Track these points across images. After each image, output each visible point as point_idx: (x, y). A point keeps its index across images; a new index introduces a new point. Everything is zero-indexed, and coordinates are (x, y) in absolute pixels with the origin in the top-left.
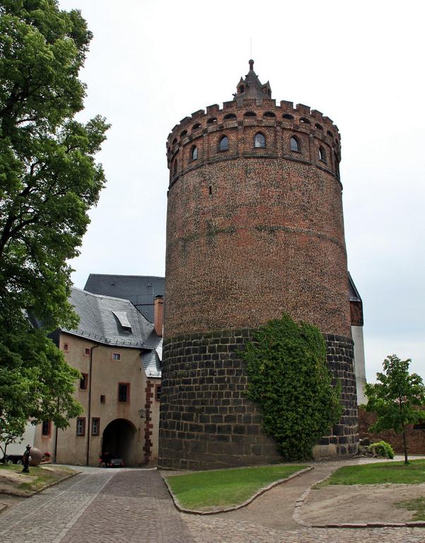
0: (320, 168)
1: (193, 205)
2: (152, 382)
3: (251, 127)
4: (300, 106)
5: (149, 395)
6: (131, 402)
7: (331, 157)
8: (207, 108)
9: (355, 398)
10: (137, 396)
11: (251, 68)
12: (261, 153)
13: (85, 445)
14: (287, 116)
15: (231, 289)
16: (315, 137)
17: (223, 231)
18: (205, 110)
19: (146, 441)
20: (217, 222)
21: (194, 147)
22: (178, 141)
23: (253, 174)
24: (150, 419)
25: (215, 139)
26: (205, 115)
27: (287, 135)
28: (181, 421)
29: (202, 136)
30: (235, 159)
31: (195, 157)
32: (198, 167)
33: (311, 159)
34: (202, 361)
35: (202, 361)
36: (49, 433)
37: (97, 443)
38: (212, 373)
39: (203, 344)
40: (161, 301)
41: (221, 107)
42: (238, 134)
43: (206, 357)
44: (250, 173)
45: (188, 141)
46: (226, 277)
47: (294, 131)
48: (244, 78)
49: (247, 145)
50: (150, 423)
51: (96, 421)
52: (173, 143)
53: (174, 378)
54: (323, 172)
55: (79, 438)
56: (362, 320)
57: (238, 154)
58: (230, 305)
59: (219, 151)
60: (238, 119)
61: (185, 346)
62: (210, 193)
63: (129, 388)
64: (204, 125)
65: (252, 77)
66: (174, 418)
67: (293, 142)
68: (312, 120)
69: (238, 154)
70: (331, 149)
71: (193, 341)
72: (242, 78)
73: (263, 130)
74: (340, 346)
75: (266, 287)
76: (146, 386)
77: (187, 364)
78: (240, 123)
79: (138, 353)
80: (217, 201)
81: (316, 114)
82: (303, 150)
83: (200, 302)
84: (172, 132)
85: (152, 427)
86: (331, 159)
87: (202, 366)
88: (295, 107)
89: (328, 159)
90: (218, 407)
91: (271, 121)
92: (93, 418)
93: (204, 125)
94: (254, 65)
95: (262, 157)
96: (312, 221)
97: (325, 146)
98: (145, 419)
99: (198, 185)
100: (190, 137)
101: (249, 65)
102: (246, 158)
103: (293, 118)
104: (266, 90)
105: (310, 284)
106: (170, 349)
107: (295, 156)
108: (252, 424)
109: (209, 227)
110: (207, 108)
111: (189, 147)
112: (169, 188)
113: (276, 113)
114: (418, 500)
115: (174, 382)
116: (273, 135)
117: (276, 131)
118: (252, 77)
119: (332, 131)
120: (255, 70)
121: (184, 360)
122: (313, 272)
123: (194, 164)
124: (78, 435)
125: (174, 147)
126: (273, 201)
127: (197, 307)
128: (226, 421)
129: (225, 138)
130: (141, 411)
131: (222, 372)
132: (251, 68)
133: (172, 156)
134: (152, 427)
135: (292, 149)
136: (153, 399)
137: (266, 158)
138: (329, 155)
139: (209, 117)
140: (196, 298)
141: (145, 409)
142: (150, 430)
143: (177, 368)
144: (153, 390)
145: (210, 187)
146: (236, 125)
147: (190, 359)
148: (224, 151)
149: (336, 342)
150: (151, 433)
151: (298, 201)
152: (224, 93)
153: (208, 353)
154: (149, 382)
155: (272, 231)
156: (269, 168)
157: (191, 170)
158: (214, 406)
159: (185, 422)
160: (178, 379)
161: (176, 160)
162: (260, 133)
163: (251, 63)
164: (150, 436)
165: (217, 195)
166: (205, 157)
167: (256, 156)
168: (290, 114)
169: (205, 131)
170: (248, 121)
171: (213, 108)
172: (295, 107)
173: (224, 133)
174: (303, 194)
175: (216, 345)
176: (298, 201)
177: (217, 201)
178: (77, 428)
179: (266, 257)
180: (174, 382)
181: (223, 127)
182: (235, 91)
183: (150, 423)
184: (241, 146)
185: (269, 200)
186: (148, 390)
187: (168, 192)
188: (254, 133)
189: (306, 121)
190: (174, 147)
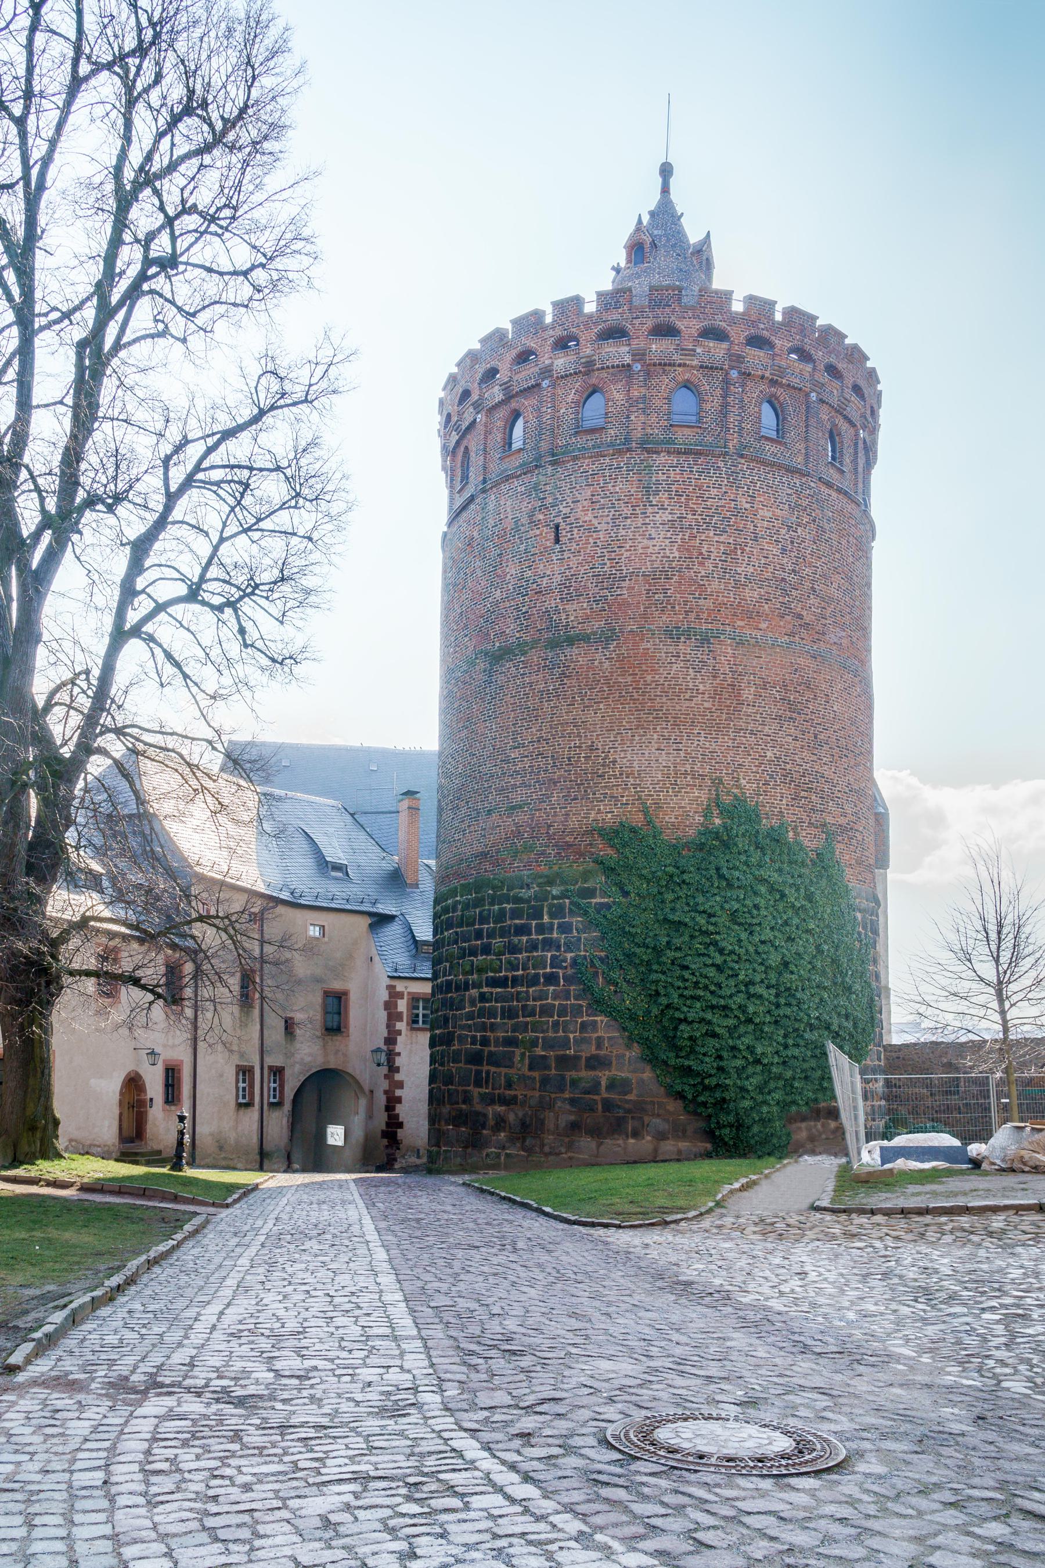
0: (829, 485)
1: (512, 570)
2: (400, 986)
3: (665, 365)
4: (792, 312)
5: (393, 1016)
6: (352, 1029)
7: (856, 453)
10: (366, 1022)
11: (665, 190)
12: (684, 436)
13: (255, 1126)
14: (757, 341)
16: (822, 401)
17: (585, 638)
18: (509, 327)
19: (389, 1117)
20: (574, 613)
21: (516, 415)
22: (475, 397)
23: (664, 496)
24: (397, 1070)
26: (545, 329)
27: (755, 391)
28: (485, 1068)
29: (538, 385)
30: (620, 452)
31: (517, 445)
32: (527, 469)
33: (806, 464)
36: (179, 1100)
37: (278, 1124)
39: (536, 898)
40: (413, 804)
41: (590, 308)
42: (629, 384)
44: (656, 493)
47: (773, 383)
48: (646, 219)
49: (654, 418)
50: (398, 1077)
51: (278, 1072)
52: (460, 403)
53: (465, 973)
54: (834, 494)
55: (242, 1111)
57: (628, 440)
61: (492, 904)
62: (557, 541)
63: (347, 1001)
65: (665, 214)
66: (468, 1062)
67: (768, 417)
68: (818, 354)
69: (628, 440)
70: (857, 435)
72: (640, 221)
75: (686, 773)
76: (384, 995)
77: (497, 942)
78: (639, 355)
79: (365, 922)
81: (831, 335)
82: (791, 435)
84: (478, 346)
85: (402, 1087)
86: (855, 461)
88: (778, 317)
89: (847, 460)
90: (571, 1036)
91: (718, 350)
92: (270, 1068)
94: (672, 181)
96: (800, 617)
97: (844, 426)
98: (384, 1070)
99: (525, 520)
100: (506, 387)
101: (660, 180)
102: (649, 451)
103: (771, 345)
104: (701, 257)
105: (788, 767)
106: (454, 910)
107: (770, 448)
108: (553, 1072)
110: (556, 305)
111: (502, 413)
112: (450, 524)
113: (732, 332)
115: (466, 983)
118: (665, 214)
119: (862, 383)
120: (674, 196)
121: (491, 935)
122: (796, 739)
123: (516, 462)
124: (240, 1105)
125: (460, 414)
126: (709, 564)
129: (597, 395)
130: (378, 1050)
132: (665, 190)
133: (455, 437)
134: (402, 1087)
135: (764, 432)
136: (402, 1026)
137: (699, 453)
138: (852, 451)
139: (559, 332)
140: (517, 798)
141: (385, 1048)
142: (398, 1093)
143: (473, 952)
144: (402, 1006)
145: (557, 527)
146: (628, 360)
147: (504, 932)
148: (593, 431)
150: (399, 1100)
151: (771, 569)
152: (588, 270)
153: (546, 919)
154: (394, 987)
155: (705, 640)
156: (704, 480)
157: (508, 478)
158: (561, 1034)
159: (493, 1069)
160: (475, 976)
161: (466, 448)
162: (687, 385)
163: (666, 171)
164: (398, 1106)
166: (544, 446)
167: (668, 437)
169: (546, 372)
170: (659, 347)
171: (568, 307)
172: (778, 317)
173: (594, 381)
174: (784, 551)
176: (771, 569)
178: (237, 1088)
179: (687, 703)
180: (466, 983)
182: (621, 258)
183: (398, 1077)
184: (637, 419)
186: (390, 1006)
187: (445, 534)
188: (672, 385)
189: (805, 356)
190: (460, 414)
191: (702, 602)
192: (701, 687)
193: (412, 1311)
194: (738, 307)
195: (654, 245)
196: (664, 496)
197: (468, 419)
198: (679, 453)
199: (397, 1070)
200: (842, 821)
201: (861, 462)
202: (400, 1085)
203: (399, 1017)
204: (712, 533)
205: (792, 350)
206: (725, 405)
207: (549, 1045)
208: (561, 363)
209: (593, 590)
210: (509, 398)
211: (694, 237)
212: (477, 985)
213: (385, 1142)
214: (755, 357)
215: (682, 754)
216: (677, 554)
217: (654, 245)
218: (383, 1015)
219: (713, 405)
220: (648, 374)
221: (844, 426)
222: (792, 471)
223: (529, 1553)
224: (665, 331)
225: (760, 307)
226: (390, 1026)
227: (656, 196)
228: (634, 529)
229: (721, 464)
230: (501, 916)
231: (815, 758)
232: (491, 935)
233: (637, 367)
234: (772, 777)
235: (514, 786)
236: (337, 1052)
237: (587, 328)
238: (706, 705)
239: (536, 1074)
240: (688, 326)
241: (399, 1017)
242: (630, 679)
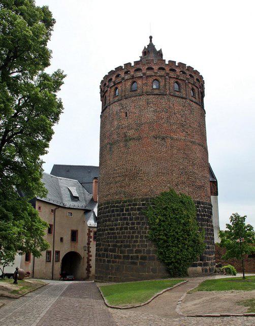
0: (192, 101)
3: (151, 76)
5: (89, 237)
6: (79, 241)
9: (213, 239)
10: (82, 238)
11: (151, 41)
12: (156, 92)
13: (51, 267)
16: (189, 83)
20: (131, 133)
21: (117, 88)
23: (152, 105)
27: (172, 81)
38: (127, 224)
41: (133, 65)
43: (123, 215)
48: (146, 47)
50: (90, 254)
51: (58, 253)
59: (132, 91)
61: (111, 208)
64: (123, 75)
67: (176, 86)
68: (187, 72)
73: (158, 78)
74: (204, 208)
78: (144, 74)
80: (130, 121)
82: (182, 90)
88: (177, 65)
93: (123, 75)
95: (157, 94)
97: (195, 88)
100: (114, 82)
104: (160, 54)
107: (177, 94)
109: (126, 136)
111: (114, 88)
112: (102, 113)
124: (47, 261)
127: (118, 184)
131: (133, 224)
132: (151, 41)
136: (92, 240)
137: (160, 95)
139: (126, 70)
140: (117, 179)
142: (90, 258)
143: (106, 221)
144: (92, 234)
146: (142, 75)
152: (134, 55)
153: (124, 212)
159: (111, 253)
163: (151, 38)
166: (123, 95)
169: (123, 79)
170: (149, 73)
172: (177, 65)
174: (182, 116)
177: (130, 121)
183: (90, 254)
186: (89, 234)
189: (184, 73)
193: (211, 189)
194: (167, 63)
195: (148, 51)
196: (152, 105)
198: (155, 95)
199: (90, 252)
201: (200, 95)
202: (91, 256)
203: (91, 237)
205: (181, 72)
206: (165, 84)
209: (135, 127)
210: (115, 84)
211: (158, 49)
212: (107, 230)
213: (87, 272)
214: (172, 74)
217: (148, 51)
218: (87, 237)
219: (162, 84)
220: (147, 78)
221: (195, 88)
222: (183, 98)
223: (164, 292)
225: (172, 63)
226: (89, 240)
227: (149, 42)
228: (144, 111)
230: (113, 211)
232: (111, 216)
236: (74, 247)
239: (122, 255)
241: (91, 237)
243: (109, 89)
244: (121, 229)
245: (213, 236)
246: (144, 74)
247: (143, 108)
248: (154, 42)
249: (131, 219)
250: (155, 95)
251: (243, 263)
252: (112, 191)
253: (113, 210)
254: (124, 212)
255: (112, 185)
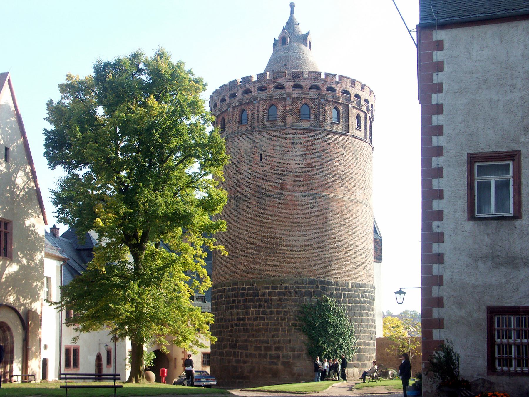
8: (257, 75)
9: (374, 332)
11: (292, 12)
15: (279, 246)
25: (265, 107)
34: (255, 303)
35: (255, 303)
38: (264, 313)
43: (258, 300)
45: (238, 104)
46: (275, 236)
47: (336, 102)
56: (381, 256)
58: (278, 259)
59: (268, 119)
60: (287, 91)
62: (261, 160)
64: (255, 93)
65: (291, 24)
66: (230, 348)
69: (285, 124)
71: (247, 287)
73: (308, 102)
74: (365, 292)
75: (308, 245)
80: (267, 168)
83: (252, 255)
87: (255, 307)
93: (255, 93)
94: (295, 8)
95: (307, 129)
101: (290, 8)
109: (260, 190)
113: (321, 86)
114: (414, 318)
116: (317, 107)
117: (319, 104)
120: (295, 15)
126: (315, 170)
127: (250, 259)
128: (276, 350)
131: (271, 313)
132: (292, 12)
137: (311, 130)
139: (259, 84)
140: (248, 252)
145: (261, 155)
146: (285, 96)
149: (361, 289)
159: (240, 351)
163: (292, 6)
165: (267, 162)
168: (333, 86)
169: (255, 98)
173: (273, 102)
175: (267, 291)
177: (267, 168)
179: (309, 220)
181: (272, 97)
185: (313, 170)
188: (301, 105)
191: (313, 183)
192: (313, 214)
197: (224, 109)
200: (362, 260)
204: (316, 159)
207: (263, 342)
208: (261, 95)
210: (241, 104)
215: (307, 238)
216: (304, 166)
220: (292, 101)
224: (298, 86)
227: (289, 15)
229: (319, 133)
231: (352, 238)
233: (288, 99)
234: (337, 246)
235: (247, 248)
237: (270, 84)
238: (315, 221)
240: (306, 85)
242: (288, 211)
243: (230, 110)
244: (255, 319)
245: (375, 328)
246: (289, 95)
247: (286, 151)
248: (297, 17)
249: (269, 307)
250: (304, 130)
251: (232, 128)
252: (240, 268)
253: (243, 293)
254: (260, 297)
255: (240, 258)
